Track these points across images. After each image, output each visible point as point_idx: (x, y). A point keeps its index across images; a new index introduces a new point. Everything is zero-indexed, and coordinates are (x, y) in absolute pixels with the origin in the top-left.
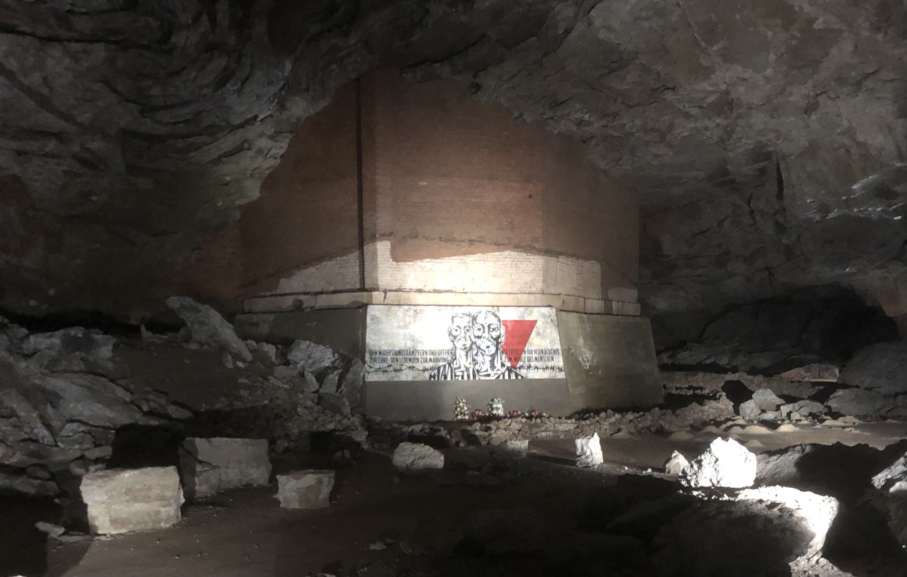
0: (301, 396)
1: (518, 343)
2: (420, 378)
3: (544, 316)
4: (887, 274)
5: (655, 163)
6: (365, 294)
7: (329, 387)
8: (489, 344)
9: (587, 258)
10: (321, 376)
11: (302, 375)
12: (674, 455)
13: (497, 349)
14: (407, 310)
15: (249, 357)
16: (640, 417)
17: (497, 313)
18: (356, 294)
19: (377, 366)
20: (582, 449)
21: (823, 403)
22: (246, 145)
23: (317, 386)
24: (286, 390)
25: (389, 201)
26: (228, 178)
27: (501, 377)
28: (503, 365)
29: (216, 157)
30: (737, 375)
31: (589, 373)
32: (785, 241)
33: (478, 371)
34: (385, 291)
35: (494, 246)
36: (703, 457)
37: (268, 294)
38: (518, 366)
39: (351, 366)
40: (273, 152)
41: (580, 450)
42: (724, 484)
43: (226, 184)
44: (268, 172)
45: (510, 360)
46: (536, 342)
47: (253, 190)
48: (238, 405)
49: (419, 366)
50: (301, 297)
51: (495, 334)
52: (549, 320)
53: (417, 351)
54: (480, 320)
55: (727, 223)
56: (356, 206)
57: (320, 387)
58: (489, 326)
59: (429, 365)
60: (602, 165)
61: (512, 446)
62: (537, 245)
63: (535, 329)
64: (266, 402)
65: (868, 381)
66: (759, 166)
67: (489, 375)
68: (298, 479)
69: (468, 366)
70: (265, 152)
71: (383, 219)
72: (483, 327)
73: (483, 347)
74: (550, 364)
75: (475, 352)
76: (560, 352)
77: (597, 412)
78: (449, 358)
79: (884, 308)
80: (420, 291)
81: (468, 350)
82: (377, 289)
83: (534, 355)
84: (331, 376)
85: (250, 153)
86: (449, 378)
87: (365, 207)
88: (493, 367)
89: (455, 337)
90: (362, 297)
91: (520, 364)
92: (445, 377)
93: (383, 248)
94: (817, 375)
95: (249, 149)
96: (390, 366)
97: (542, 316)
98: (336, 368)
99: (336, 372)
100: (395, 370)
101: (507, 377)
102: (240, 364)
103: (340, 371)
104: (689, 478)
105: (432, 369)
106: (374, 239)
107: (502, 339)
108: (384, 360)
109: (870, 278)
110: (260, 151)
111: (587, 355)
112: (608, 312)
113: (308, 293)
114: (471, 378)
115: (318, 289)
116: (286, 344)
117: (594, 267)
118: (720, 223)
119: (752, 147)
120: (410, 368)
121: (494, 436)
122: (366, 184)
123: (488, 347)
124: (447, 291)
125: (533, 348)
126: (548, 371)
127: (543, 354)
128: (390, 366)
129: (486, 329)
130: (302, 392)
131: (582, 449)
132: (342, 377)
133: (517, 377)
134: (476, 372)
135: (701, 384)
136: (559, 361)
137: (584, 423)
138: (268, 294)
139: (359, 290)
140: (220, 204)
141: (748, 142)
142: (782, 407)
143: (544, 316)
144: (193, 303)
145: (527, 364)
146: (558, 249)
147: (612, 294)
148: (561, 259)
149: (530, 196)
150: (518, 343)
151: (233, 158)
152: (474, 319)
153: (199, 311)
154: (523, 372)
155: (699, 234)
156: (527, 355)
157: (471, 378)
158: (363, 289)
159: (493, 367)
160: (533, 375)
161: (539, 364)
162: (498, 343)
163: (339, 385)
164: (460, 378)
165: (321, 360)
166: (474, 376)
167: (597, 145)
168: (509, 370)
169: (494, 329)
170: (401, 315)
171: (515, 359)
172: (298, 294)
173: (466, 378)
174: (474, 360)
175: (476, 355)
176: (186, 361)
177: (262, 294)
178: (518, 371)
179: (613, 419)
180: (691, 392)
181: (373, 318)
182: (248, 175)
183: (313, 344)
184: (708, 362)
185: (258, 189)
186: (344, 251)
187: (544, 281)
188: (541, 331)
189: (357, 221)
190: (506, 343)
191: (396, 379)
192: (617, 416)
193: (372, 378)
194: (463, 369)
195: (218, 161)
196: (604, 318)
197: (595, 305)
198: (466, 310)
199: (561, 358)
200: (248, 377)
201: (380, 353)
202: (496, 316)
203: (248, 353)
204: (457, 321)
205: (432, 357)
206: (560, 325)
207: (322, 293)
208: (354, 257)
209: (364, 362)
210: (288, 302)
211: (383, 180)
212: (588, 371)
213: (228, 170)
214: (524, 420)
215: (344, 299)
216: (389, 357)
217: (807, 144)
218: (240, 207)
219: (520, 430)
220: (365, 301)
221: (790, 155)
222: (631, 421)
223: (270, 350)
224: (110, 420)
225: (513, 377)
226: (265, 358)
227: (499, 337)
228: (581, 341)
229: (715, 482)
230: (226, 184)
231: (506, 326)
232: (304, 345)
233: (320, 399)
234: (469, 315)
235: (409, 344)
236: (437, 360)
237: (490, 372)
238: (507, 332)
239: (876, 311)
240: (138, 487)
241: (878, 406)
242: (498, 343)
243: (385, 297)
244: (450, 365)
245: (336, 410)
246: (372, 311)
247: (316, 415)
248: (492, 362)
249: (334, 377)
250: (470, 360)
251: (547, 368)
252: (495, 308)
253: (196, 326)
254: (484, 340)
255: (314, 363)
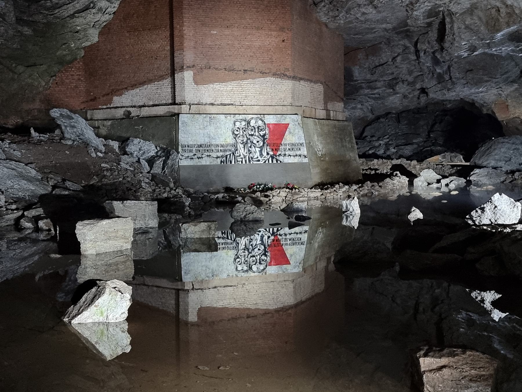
0: (141, 175)
1: (277, 139)
2: (215, 163)
3: (293, 120)
4: (501, 92)
5: (362, 19)
6: (176, 106)
7: (157, 169)
8: (259, 139)
9: (316, 82)
10: (151, 162)
11: (138, 161)
12: (413, 210)
13: (264, 143)
14: (205, 117)
15: (103, 149)
16: (359, 187)
17: (263, 119)
18: (170, 106)
19: (186, 155)
20: (347, 207)
21: (466, 178)
22: (92, 5)
23: (149, 169)
24: (131, 171)
25: (192, 44)
26: (79, 28)
27: (267, 162)
28: (268, 154)
29: (72, 13)
30: (400, 160)
31: (321, 159)
32: (438, 71)
33: (252, 158)
34: (190, 105)
35: (259, 74)
36: (485, 205)
37: (105, 107)
38: (278, 154)
39: (170, 155)
40: (109, 9)
41: (345, 208)
42: (500, 222)
43: (77, 32)
44: (105, 24)
45: (273, 150)
46: (289, 138)
47: (94, 36)
48: (105, 181)
49: (214, 155)
50: (129, 109)
51: (262, 133)
52: (297, 123)
53: (212, 145)
54: (253, 123)
55: (399, 59)
56: (169, 48)
57: (151, 169)
58: (258, 128)
59: (220, 154)
60: (324, 19)
61: (296, 206)
62: (287, 73)
63: (288, 130)
64: (121, 179)
65: (493, 163)
66: (428, 20)
67: (259, 161)
68: (195, 226)
69: (246, 155)
70: (104, 10)
71: (188, 56)
72: (255, 129)
73: (255, 142)
74: (298, 153)
75: (249, 145)
76: (305, 144)
77: (332, 184)
78: (233, 149)
79: (497, 115)
80: (212, 104)
81: (245, 144)
82: (184, 103)
83: (288, 147)
84: (158, 162)
85: (94, 11)
86: (233, 163)
87: (176, 48)
88: (261, 155)
89: (236, 135)
90: (175, 109)
91: (279, 153)
92: (231, 162)
93: (188, 75)
94: (450, 160)
95: (93, 8)
96: (195, 155)
97: (292, 121)
98: (160, 157)
99: (161, 160)
100: (198, 158)
101: (270, 162)
102: (99, 154)
103: (164, 158)
104: (474, 219)
105: (222, 157)
106: (182, 69)
107: (267, 136)
108: (191, 151)
109: (486, 95)
110: (100, 10)
111: (320, 147)
112: (328, 119)
113: (135, 107)
114: (248, 163)
115: (141, 104)
116: (124, 141)
117: (319, 88)
118: (394, 59)
119: (430, 8)
120: (208, 156)
121: (272, 200)
122: (176, 33)
123: (258, 142)
124: (229, 105)
125: (287, 142)
126: (298, 157)
127: (294, 146)
128: (195, 155)
129: (257, 130)
130: (142, 173)
131: (347, 207)
132: (165, 162)
133: (277, 162)
134: (251, 159)
135: (377, 167)
136: (304, 151)
137: (326, 191)
138: (105, 107)
139: (171, 104)
140: (73, 46)
141: (429, 4)
142: (442, 181)
143: (293, 120)
144: (69, 113)
145: (283, 153)
146: (300, 76)
147: (330, 107)
148: (302, 82)
149: (283, 41)
150: (277, 139)
151: (83, 14)
152: (249, 123)
153: (73, 119)
154: (281, 158)
155: (379, 66)
156: (283, 147)
157: (248, 163)
158: (174, 103)
159: (261, 155)
160: (287, 160)
161: (291, 153)
162: (264, 139)
163: (163, 169)
164: (240, 163)
165: (149, 151)
166: (250, 161)
167: (324, 6)
168: (272, 157)
169: (261, 130)
170: (201, 121)
171: (276, 150)
172: (127, 107)
173: (244, 162)
174: (249, 151)
175: (250, 147)
176: (67, 152)
177: (100, 107)
178: (278, 158)
179: (344, 189)
180: (373, 172)
181: (184, 122)
182: (92, 26)
183: (142, 141)
184: (370, 152)
185: (97, 36)
186: (161, 78)
187: (293, 97)
188: (292, 131)
189: (169, 58)
190: (269, 139)
191: (199, 164)
192: (347, 187)
193: (184, 163)
194: (242, 156)
195: (72, 16)
196: (327, 122)
197: (322, 114)
198: (241, 117)
199: (305, 149)
200: (106, 162)
201: (188, 146)
202: (263, 121)
203: (103, 147)
204: (238, 124)
205: (222, 148)
206: (304, 127)
207: (144, 106)
208: (167, 82)
209: (178, 153)
210: (120, 113)
211: (188, 31)
212: (320, 157)
213: (79, 22)
214: (288, 190)
215: (161, 111)
216: (194, 149)
217: (469, 6)
218: (84, 48)
219: (286, 197)
220: (176, 112)
221: (456, 13)
222: (355, 190)
223: (115, 145)
224: (33, 191)
225: (275, 161)
226: (112, 150)
227: (265, 135)
228: (316, 138)
229: (493, 221)
230: (77, 32)
231: (269, 127)
232: (136, 141)
233: (154, 178)
234: (245, 121)
235: (207, 141)
236: (225, 151)
237: (259, 158)
238: (270, 131)
239: (492, 118)
240: (111, 230)
241: (502, 179)
242: (264, 139)
243: (190, 109)
244: (233, 154)
245: (166, 184)
246: (182, 118)
247: (153, 188)
248: (261, 151)
249: (159, 163)
250: (246, 150)
251: (296, 155)
252: (262, 116)
253: (68, 129)
254: (256, 137)
255: (144, 153)
